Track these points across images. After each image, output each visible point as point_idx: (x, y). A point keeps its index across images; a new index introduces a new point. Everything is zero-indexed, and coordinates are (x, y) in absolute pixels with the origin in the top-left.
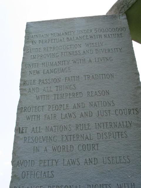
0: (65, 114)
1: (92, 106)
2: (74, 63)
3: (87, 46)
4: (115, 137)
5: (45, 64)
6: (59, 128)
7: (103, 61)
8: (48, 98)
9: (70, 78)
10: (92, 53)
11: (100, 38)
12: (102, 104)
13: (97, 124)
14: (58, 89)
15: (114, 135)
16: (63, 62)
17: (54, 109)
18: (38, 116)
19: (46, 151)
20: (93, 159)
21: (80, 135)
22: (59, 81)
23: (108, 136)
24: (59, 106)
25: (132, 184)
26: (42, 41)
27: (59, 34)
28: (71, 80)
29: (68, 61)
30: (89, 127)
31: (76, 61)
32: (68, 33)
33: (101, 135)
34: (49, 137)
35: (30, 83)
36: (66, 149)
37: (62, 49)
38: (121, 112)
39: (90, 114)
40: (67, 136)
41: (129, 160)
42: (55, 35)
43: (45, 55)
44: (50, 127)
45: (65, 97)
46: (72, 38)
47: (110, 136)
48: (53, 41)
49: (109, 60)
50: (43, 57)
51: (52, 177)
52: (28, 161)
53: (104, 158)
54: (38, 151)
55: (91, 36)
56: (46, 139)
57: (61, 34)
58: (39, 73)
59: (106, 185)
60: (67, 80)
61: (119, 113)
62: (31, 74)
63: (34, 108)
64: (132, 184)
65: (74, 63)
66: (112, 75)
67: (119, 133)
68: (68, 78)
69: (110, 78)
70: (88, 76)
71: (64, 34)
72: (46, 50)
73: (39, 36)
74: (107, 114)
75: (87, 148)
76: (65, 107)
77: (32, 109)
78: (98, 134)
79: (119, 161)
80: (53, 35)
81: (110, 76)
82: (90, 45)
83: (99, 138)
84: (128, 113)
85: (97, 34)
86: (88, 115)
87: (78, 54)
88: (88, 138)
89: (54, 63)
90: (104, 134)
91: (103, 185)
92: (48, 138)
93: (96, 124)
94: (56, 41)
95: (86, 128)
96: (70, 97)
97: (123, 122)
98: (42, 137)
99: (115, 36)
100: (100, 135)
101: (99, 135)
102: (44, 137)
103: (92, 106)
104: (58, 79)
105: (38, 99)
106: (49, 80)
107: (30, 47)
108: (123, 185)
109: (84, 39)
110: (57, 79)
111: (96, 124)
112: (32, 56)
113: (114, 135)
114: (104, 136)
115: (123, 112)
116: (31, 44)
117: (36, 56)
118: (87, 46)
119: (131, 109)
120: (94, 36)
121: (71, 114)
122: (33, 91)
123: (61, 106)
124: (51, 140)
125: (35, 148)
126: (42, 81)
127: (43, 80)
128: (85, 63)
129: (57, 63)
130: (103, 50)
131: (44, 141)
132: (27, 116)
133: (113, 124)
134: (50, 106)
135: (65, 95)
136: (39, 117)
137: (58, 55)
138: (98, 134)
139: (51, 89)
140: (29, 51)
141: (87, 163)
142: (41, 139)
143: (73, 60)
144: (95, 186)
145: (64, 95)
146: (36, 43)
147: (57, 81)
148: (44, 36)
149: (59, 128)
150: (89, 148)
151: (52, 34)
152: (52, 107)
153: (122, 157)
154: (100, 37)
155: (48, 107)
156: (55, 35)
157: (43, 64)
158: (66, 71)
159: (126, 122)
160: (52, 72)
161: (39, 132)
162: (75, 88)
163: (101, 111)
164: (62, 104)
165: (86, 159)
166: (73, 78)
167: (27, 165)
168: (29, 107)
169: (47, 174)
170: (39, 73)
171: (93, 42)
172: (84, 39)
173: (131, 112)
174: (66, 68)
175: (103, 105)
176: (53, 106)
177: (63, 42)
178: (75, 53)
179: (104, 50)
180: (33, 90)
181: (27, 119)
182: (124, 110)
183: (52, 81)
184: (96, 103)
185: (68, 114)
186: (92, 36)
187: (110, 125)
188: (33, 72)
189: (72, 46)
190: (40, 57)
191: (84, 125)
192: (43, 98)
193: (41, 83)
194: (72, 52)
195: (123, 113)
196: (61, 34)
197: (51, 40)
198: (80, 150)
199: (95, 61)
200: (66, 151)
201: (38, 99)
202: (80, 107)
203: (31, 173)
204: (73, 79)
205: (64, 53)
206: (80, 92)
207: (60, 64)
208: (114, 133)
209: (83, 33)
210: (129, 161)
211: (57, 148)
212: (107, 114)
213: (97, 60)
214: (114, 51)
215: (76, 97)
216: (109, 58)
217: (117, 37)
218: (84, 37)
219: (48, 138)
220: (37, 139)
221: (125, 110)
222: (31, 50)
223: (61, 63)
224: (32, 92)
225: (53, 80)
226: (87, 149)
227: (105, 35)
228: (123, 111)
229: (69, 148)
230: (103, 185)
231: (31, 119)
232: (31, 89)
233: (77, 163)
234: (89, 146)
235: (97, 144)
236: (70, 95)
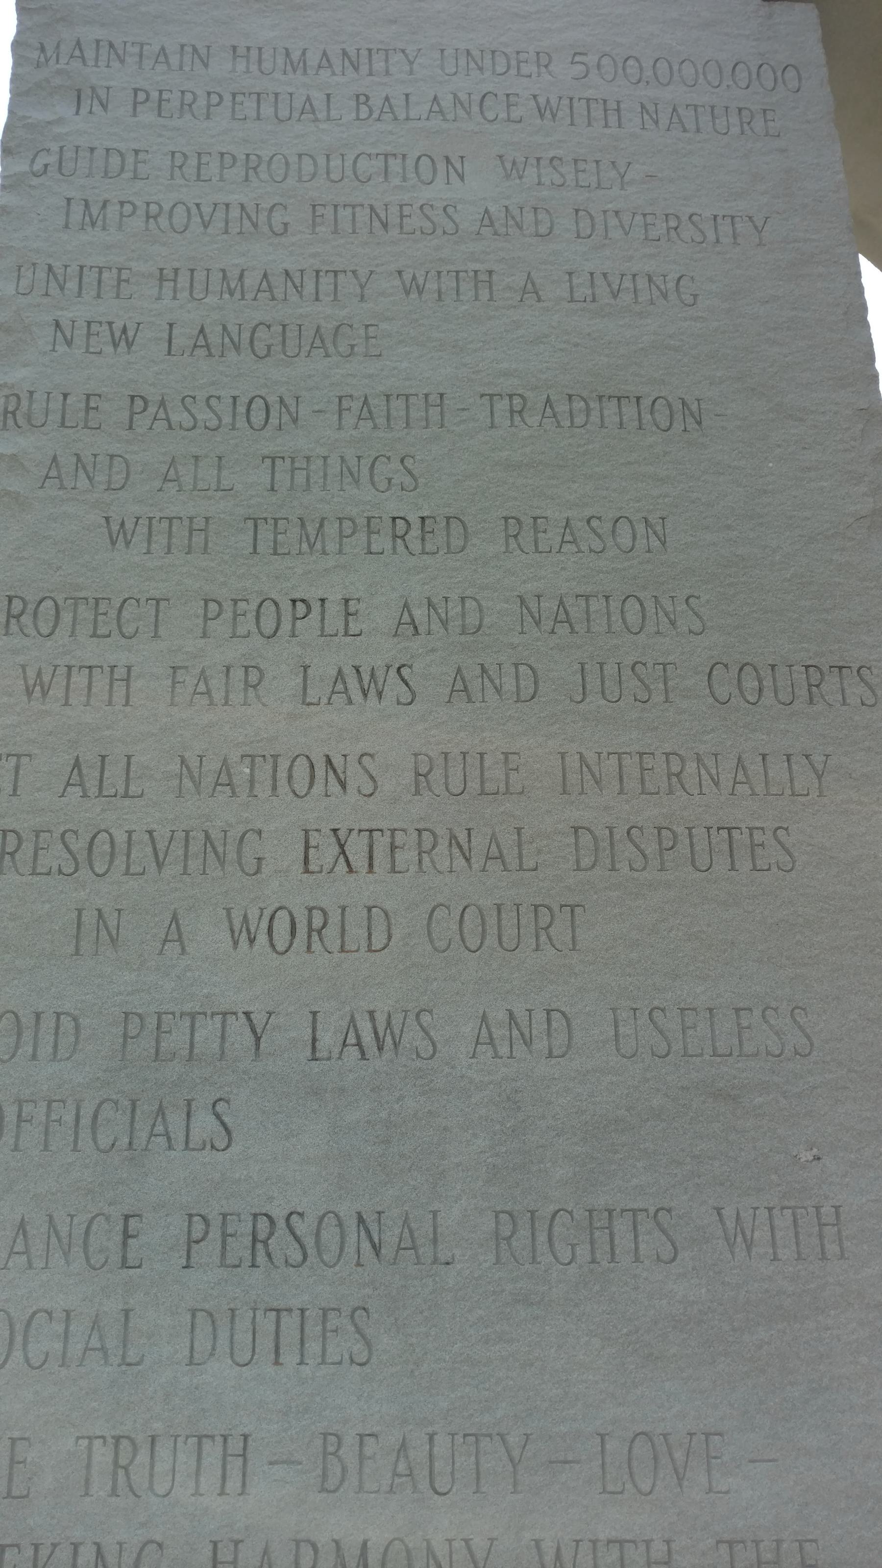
0: (334, 673)
1: (538, 623)
2: (407, 293)
3: (508, 176)
4: (703, 861)
5: (183, 280)
6: (282, 775)
7: (626, 298)
8: (198, 539)
9: (378, 404)
10: (543, 230)
11: (606, 126)
12: (616, 617)
13: (573, 762)
14: (282, 477)
15: (701, 845)
16: (326, 281)
17: (247, 624)
18: (120, 673)
19: (370, 424)
20: (540, 1016)
21: (441, 831)
22: (286, 418)
23: (651, 849)
24: (286, 606)
25: (827, 1210)
26: (155, 95)
27: (296, 55)
28: (381, 421)
29: (363, 273)
30: (513, 775)
31: (421, 281)
32: (364, 60)
33: (606, 844)
34: (202, 836)
35: (56, 417)
36: (332, 933)
37: (314, 176)
38: (750, 684)
39: (523, 683)
40: (342, 834)
41: (809, 1038)
42: (260, 61)
43: (180, 210)
44: (212, 765)
45: (331, 547)
46: (398, 102)
47: (668, 856)
48: (250, 105)
49: (672, 296)
50: (163, 221)
51: (221, 1144)
52: (27, 1019)
53: (623, 1015)
54: (113, 941)
55: (542, 100)
56: (177, 850)
57: (313, 58)
58: (129, 345)
59: (634, 1211)
60: (349, 419)
61: (736, 692)
62: (62, 348)
63: (86, 614)
64: (827, 1210)
65: (407, 293)
66: (694, 407)
67: (735, 834)
68: (356, 405)
69: (678, 426)
70: (517, 401)
71: (336, 62)
72: (190, 170)
73: (136, 50)
74: (647, 687)
75: (492, 931)
76: (334, 621)
77: (67, 617)
78: (576, 829)
79: (736, 1041)
80: (247, 58)
81: (678, 417)
82: (531, 172)
83: (586, 862)
84: (803, 692)
85: (590, 93)
86: (506, 687)
87: (439, 231)
88: (501, 857)
89: (252, 280)
90: (620, 833)
91: (610, 1212)
92: (196, 847)
93: (563, 755)
94: (267, 110)
95: (490, 787)
96: (375, 548)
97: (764, 756)
98: (150, 832)
99: (721, 124)
100: (595, 838)
101: (586, 839)
102: (162, 834)
103: (538, 623)
104: (282, 401)
105: (120, 544)
106: (213, 402)
107: (58, 130)
108: (763, 1214)
109: (490, 115)
110: (273, 399)
111: (563, 755)
112: (77, 211)
113: (701, 845)
114: (627, 851)
115: (768, 683)
116: (66, 109)
117: (104, 206)
118: (508, 176)
119: (825, 669)
120: (566, 102)
121: (380, 674)
122: (83, 482)
123: (301, 608)
124: (222, 861)
125: (90, 918)
126: (152, 410)
127: (162, 404)
128: (491, 299)
129: (278, 281)
130: (626, 218)
131: (160, 865)
132: (24, 667)
133: (691, 767)
134: (213, 606)
135: (331, 529)
136: (128, 680)
137: (286, 225)
138: (576, 829)
139: (225, 473)
140: (53, 159)
141: (491, 1042)
142: (142, 853)
143: (400, 273)
144: (551, 1226)
145: (327, 528)
146: (104, 107)
147: (274, 421)
148: (174, 60)
149: (282, 775)
150: (510, 932)
151: (241, 51)
152: (228, 615)
153: (757, 1013)
154: (613, 119)
155: (201, 612)
156: (260, 61)
157: (162, 279)
158: (343, 348)
159: (789, 757)
160: (237, 348)
161: (126, 795)
162: (408, 480)
163: (601, 665)
164: (313, 594)
165: (484, 1018)
166: (401, 403)
167: (17, 1047)
168: (49, 603)
169: (176, 1120)
170: (129, 345)
171: (560, 153)
172: (490, 115)
173: (824, 687)
174: (345, 330)
175: (618, 625)
176: (235, 601)
177: (323, 126)
178: (415, 222)
179: (639, 218)
180: (82, 474)
181: (29, 693)
182: (773, 667)
183: (234, 415)
184: (569, 601)
185: (371, 1013)
186: (554, 102)
187: (670, 775)
188: (81, 332)
189: (395, 165)
190: (137, 223)
191: (473, 760)
192: (160, 540)
193: (142, 422)
194: (394, 210)
195: (768, 693)
196: (313, 58)
197: (227, 97)
198: (442, 944)
199: (567, 295)
200: (336, 945)
201: (120, 544)
202: (444, 623)
203: (48, 1115)
204: (394, 413)
205: (329, 212)
206: (450, 511)
207: (299, 289)
208: (699, 832)
209: (481, 69)
210: (804, 1040)
211: (264, 925)
212: (647, 687)
213: (583, 292)
214: (711, 236)
215: (416, 546)
216: (671, 285)
217: (735, 130)
218: (488, 102)
219: (196, 847)
220: (102, 845)
221: (782, 670)
222: (69, 154)
223: (309, 288)
224: (68, 483)
225: (241, 409)
226: (491, 940)
227: (651, 108)
228: (766, 673)
229: (356, 933)
230: (610, 1212)
231: (57, 692)
232: (67, 462)
233: (412, 1037)
234: (510, 920)
235: (573, 908)
236: (370, 533)
